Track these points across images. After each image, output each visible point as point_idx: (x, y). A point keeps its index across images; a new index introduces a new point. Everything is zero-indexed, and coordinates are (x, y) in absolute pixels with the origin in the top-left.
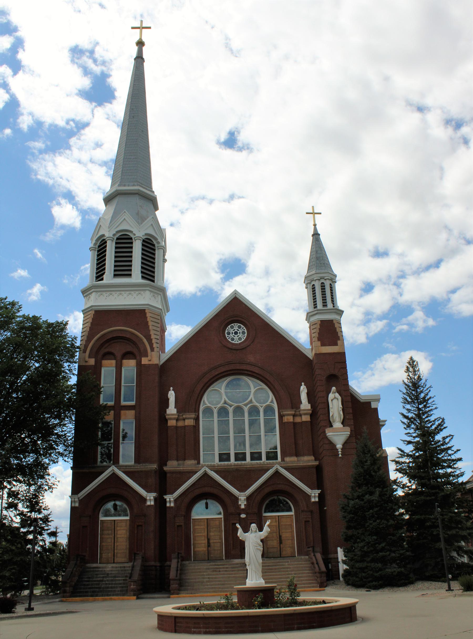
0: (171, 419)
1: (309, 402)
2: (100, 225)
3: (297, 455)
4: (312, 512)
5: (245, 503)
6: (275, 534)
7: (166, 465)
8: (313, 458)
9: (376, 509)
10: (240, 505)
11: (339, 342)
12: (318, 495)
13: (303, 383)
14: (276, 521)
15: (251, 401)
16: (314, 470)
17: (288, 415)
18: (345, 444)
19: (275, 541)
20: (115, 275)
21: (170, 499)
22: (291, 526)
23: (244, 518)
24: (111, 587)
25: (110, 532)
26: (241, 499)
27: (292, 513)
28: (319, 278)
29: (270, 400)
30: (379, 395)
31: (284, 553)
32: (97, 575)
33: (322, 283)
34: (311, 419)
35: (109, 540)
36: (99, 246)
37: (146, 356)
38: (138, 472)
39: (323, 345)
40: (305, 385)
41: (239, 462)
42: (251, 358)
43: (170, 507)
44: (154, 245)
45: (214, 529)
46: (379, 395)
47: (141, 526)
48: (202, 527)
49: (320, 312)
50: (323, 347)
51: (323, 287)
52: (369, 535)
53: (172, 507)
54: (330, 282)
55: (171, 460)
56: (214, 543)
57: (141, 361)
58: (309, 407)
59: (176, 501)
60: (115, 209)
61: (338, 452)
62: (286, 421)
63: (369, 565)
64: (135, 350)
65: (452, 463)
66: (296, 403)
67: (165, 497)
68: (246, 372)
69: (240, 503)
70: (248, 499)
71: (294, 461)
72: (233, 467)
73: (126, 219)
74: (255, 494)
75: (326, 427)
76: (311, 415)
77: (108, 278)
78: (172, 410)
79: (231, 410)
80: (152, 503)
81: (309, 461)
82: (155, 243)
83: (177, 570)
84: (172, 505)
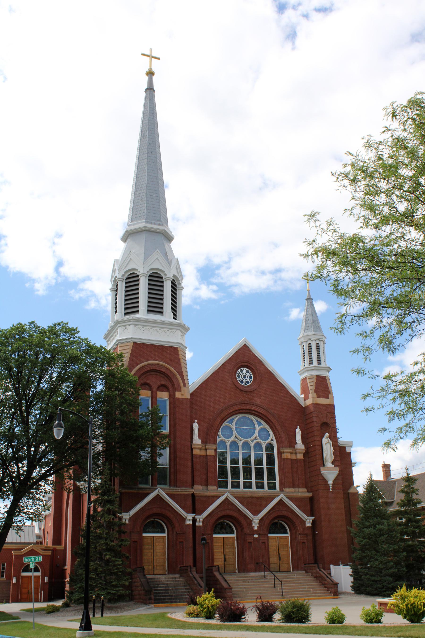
0: (196, 448)
1: (303, 442)
2: (131, 259)
3: (294, 487)
4: (307, 535)
5: (258, 525)
6: (275, 552)
8: (306, 490)
9: (386, 536)
10: (254, 527)
11: (330, 395)
12: (312, 521)
13: (298, 427)
14: (276, 542)
15: (256, 439)
16: (308, 500)
17: (287, 452)
18: (335, 481)
19: (276, 558)
22: (287, 545)
23: (256, 538)
24: (181, 595)
25: (150, 547)
27: (288, 535)
28: (316, 339)
29: (270, 438)
30: (352, 442)
31: (282, 568)
32: (158, 584)
33: (318, 343)
34: (304, 457)
35: (149, 554)
36: (127, 279)
37: (180, 390)
38: (178, 494)
39: (318, 397)
40: (300, 428)
41: (247, 490)
42: (257, 401)
43: (199, 527)
45: (229, 546)
46: (352, 442)
47: (182, 542)
48: (219, 544)
49: (316, 369)
50: (319, 399)
52: (381, 556)
55: (196, 485)
56: (229, 558)
57: (174, 394)
58: (303, 447)
60: (145, 246)
61: (329, 487)
62: (285, 457)
63: (383, 578)
64: (168, 384)
65: (402, 501)
66: (292, 443)
68: (254, 412)
69: (253, 525)
70: (261, 521)
71: (292, 492)
72: (248, 494)
73: (159, 258)
74: (265, 518)
75: (320, 466)
76: (304, 454)
78: (197, 441)
79: (240, 444)
81: (303, 492)
82: (162, 275)
84: (201, 524)
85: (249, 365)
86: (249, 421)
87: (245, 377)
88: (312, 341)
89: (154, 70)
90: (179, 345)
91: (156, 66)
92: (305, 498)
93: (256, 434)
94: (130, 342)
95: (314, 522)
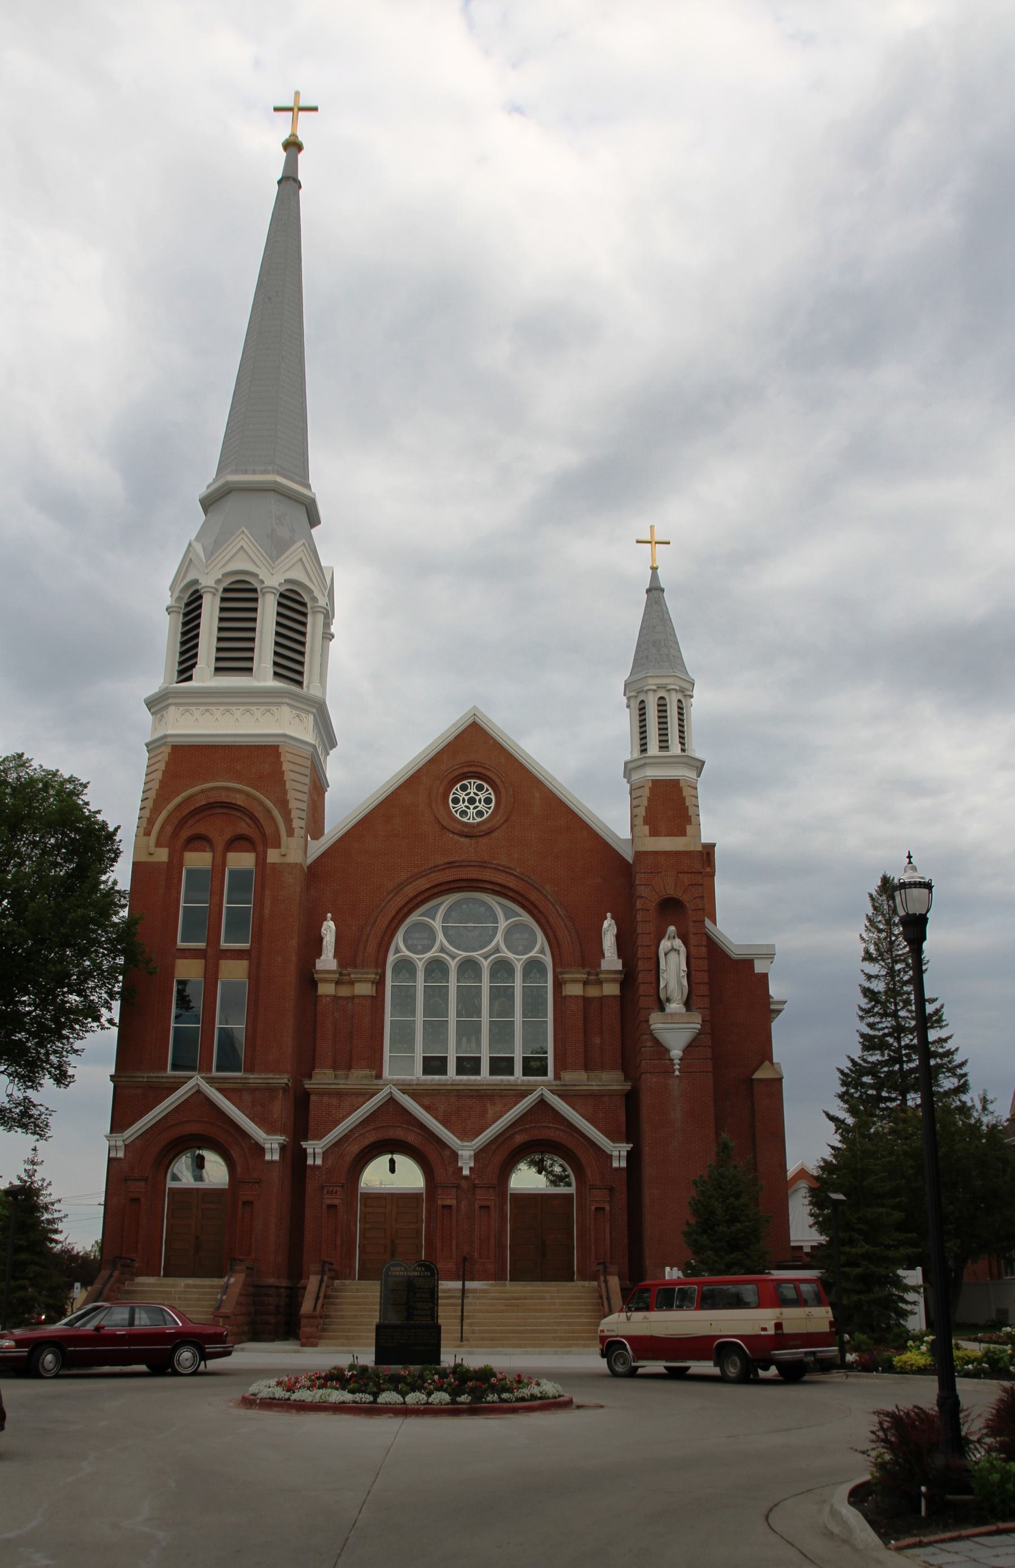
1: (621, 954)
3: (587, 1068)
4: (611, 1190)
7: (310, 1077)
11: (689, 828)
13: (609, 915)
15: (497, 950)
17: (574, 981)
20: (218, 670)
21: (314, 1149)
24: (355, 1316)
26: (462, 1156)
30: (774, 945)
36: (187, 605)
37: (278, 845)
39: (654, 833)
40: (612, 918)
43: (314, 1167)
44: (304, 605)
49: (656, 761)
51: (662, 707)
53: (319, 1167)
54: (680, 696)
58: (618, 965)
59: (325, 1154)
67: (304, 1144)
70: (477, 1156)
73: (246, 547)
77: (204, 676)
78: (327, 961)
79: (453, 965)
80: (276, 1157)
82: (306, 599)
83: (317, 1298)
84: (319, 1162)
85: (484, 771)
86: (483, 909)
87: (472, 801)
88: (669, 690)
89: (301, 138)
90: (282, 739)
91: (307, 129)
92: (611, 1094)
93: (499, 937)
94: (165, 744)
95: (633, 1157)
